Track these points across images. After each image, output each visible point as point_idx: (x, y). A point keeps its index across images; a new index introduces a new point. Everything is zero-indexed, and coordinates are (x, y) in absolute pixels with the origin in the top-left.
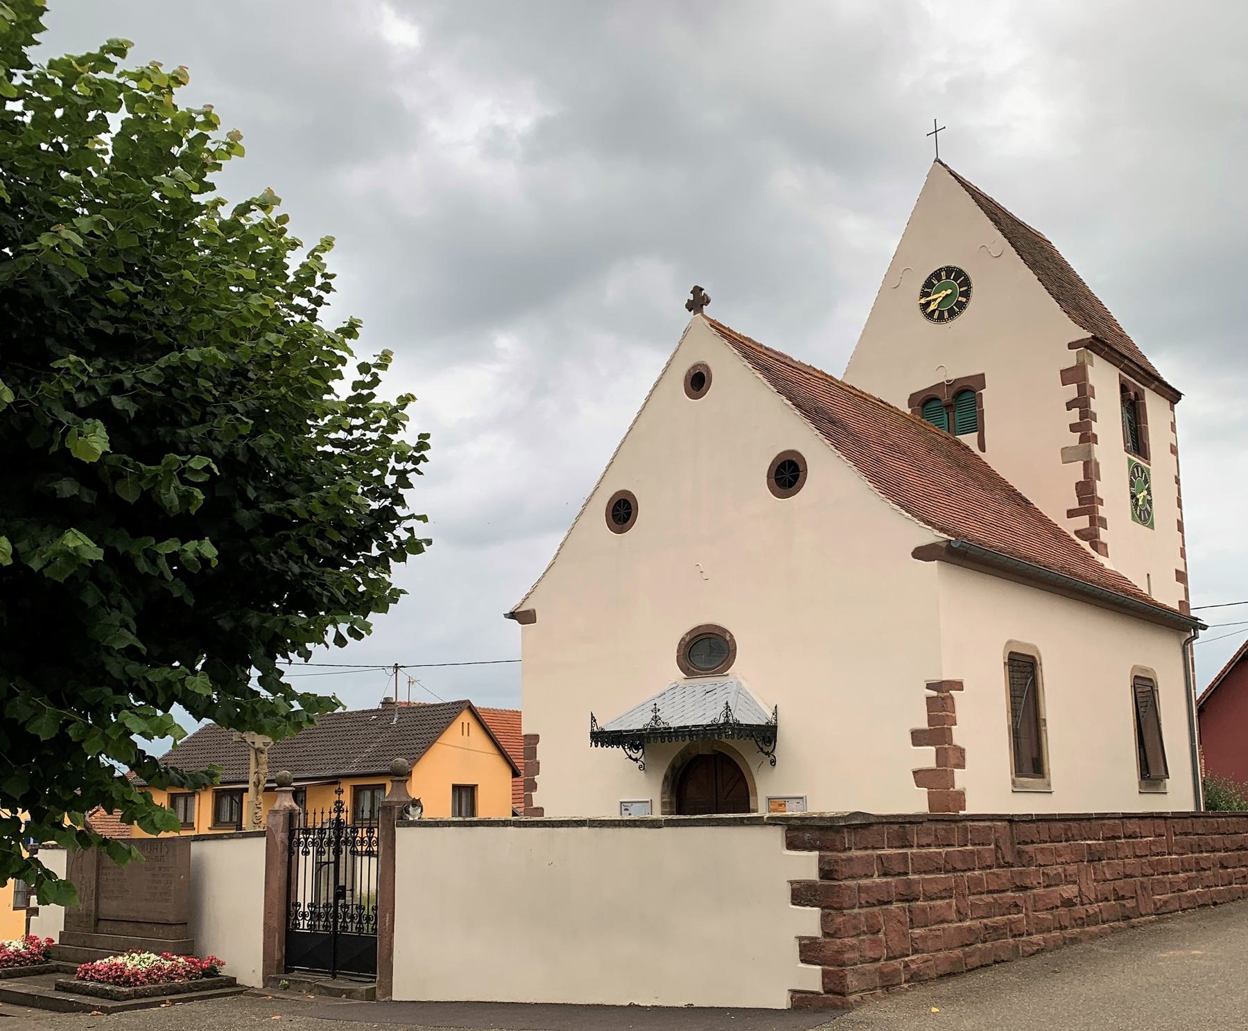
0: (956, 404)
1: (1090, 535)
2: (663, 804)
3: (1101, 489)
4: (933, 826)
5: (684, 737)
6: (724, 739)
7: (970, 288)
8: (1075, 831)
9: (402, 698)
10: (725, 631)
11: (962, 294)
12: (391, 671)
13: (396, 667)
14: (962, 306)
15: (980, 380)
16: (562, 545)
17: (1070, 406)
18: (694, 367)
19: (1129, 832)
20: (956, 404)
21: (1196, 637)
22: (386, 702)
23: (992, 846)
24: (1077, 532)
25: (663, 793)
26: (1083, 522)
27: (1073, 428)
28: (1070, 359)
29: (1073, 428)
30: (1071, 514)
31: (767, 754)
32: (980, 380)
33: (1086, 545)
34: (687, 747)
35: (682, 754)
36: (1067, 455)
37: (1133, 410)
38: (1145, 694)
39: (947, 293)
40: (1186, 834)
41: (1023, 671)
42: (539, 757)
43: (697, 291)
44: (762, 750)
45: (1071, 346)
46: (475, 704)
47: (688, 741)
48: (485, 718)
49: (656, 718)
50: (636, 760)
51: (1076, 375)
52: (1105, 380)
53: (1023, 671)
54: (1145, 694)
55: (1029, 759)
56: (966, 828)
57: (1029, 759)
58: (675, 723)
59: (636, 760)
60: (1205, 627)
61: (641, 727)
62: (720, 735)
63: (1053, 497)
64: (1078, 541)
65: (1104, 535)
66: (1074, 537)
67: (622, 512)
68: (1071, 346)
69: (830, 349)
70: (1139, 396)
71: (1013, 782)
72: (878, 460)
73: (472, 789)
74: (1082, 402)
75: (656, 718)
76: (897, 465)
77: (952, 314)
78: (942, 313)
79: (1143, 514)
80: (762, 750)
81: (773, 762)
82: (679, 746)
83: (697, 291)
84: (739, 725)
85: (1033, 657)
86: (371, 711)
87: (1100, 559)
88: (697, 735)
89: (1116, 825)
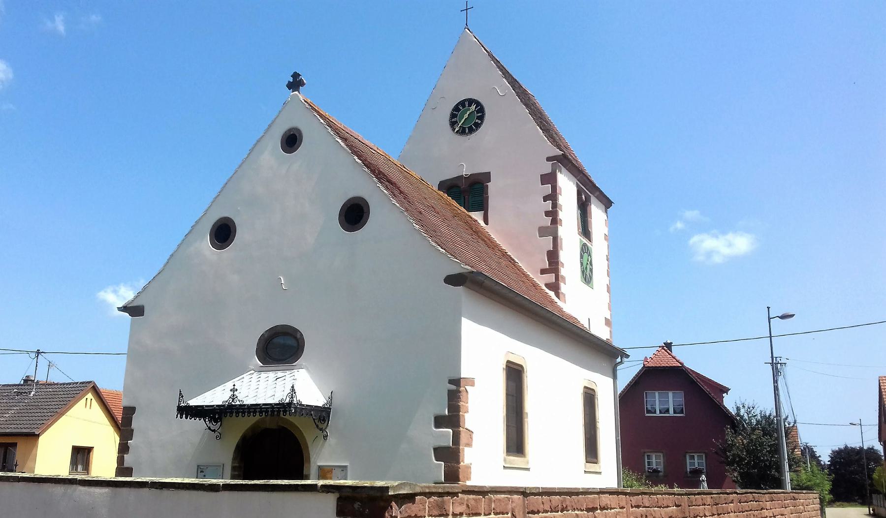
0: (470, 192)
1: (555, 287)
2: (234, 468)
3: (563, 256)
4: (466, 497)
5: (255, 412)
6: (287, 417)
7: (482, 123)
8: (568, 503)
9: (41, 377)
10: (296, 331)
11: (478, 118)
12: (33, 355)
13: (38, 353)
14: (478, 126)
15: (487, 176)
16: (172, 255)
17: (546, 199)
18: (290, 130)
19: (603, 505)
20: (470, 192)
21: (621, 362)
22: (27, 380)
23: (510, 515)
24: (546, 285)
25: (234, 459)
26: (551, 278)
27: (547, 214)
28: (547, 168)
29: (547, 214)
30: (543, 272)
31: (321, 429)
32: (487, 176)
33: (552, 294)
34: (258, 422)
35: (253, 428)
36: (543, 232)
37: (583, 207)
38: (590, 398)
39: (467, 117)
40: (638, 507)
41: (515, 375)
42: (134, 425)
43: (296, 75)
44: (317, 426)
45: (549, 159)
46: (101, 386)
47: (258, 417)
48: (105, 396)
49: (233, 397)
50: (214, 431)
51: (549, 179)
52: (567, 186)
53: (515, 375)
54: (590, 398)
55: (516, 444)
56: (490, 499)
57: (516, 444)
58: (249, 401)
59: (214, 431)
60: (628, 356)
61: (220, 403)
62: (285, 412)
63: (531, 265)
64: (547, 291)
65: (563, 288)
66: (544, 288)
67: (223, 233)
68: (549, 159)
69: (389, 146)
70: (588, 200)
71: (505, 460)
72: (421, 213)
73: (89, 450)
74: (553, 197)
75: (233, 397)
76: (433, 219)
77: (471, 130)
78: (464, 129)
79: (587, 277)
80: (317, 426)
81: (325, 437)
82: (248, 422)
83: (296, 75)
84: (301, 405)
85: (521, 366)
86: (15, 385)
87: (560, 303)
88: (267, 412)
89: (594, 499)
